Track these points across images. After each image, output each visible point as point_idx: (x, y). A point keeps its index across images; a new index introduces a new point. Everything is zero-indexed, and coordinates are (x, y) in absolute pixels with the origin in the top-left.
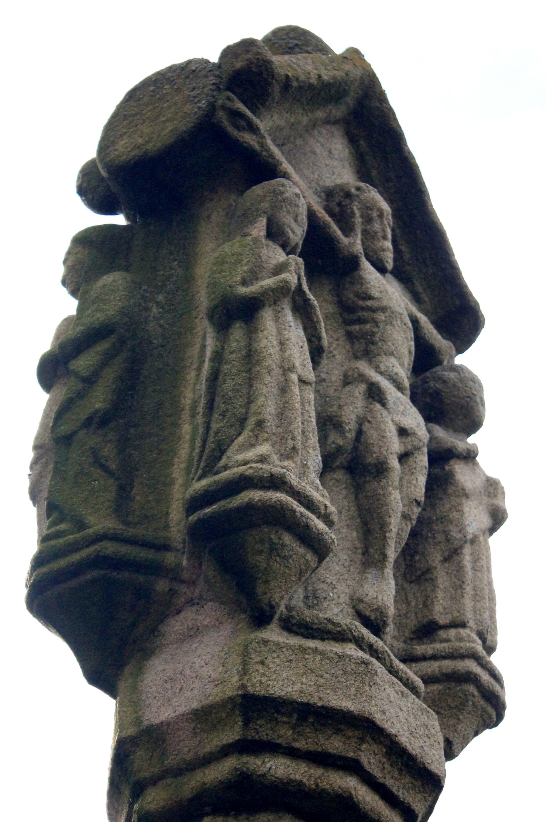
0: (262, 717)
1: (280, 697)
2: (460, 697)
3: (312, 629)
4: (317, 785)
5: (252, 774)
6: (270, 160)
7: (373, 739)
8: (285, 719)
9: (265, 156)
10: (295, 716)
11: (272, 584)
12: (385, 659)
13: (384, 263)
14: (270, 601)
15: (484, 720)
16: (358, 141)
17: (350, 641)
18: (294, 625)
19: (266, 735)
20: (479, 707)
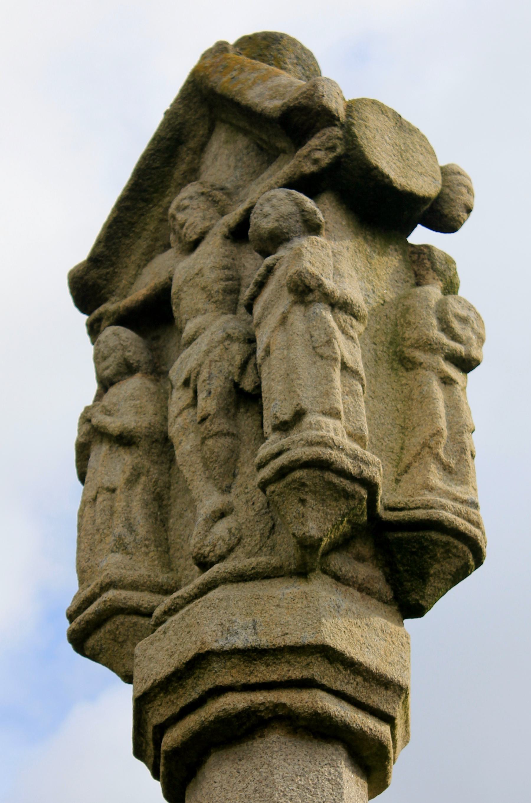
7: (149, 703)
12: (177, 604)
15: (295, 488)
20: (282, 490)
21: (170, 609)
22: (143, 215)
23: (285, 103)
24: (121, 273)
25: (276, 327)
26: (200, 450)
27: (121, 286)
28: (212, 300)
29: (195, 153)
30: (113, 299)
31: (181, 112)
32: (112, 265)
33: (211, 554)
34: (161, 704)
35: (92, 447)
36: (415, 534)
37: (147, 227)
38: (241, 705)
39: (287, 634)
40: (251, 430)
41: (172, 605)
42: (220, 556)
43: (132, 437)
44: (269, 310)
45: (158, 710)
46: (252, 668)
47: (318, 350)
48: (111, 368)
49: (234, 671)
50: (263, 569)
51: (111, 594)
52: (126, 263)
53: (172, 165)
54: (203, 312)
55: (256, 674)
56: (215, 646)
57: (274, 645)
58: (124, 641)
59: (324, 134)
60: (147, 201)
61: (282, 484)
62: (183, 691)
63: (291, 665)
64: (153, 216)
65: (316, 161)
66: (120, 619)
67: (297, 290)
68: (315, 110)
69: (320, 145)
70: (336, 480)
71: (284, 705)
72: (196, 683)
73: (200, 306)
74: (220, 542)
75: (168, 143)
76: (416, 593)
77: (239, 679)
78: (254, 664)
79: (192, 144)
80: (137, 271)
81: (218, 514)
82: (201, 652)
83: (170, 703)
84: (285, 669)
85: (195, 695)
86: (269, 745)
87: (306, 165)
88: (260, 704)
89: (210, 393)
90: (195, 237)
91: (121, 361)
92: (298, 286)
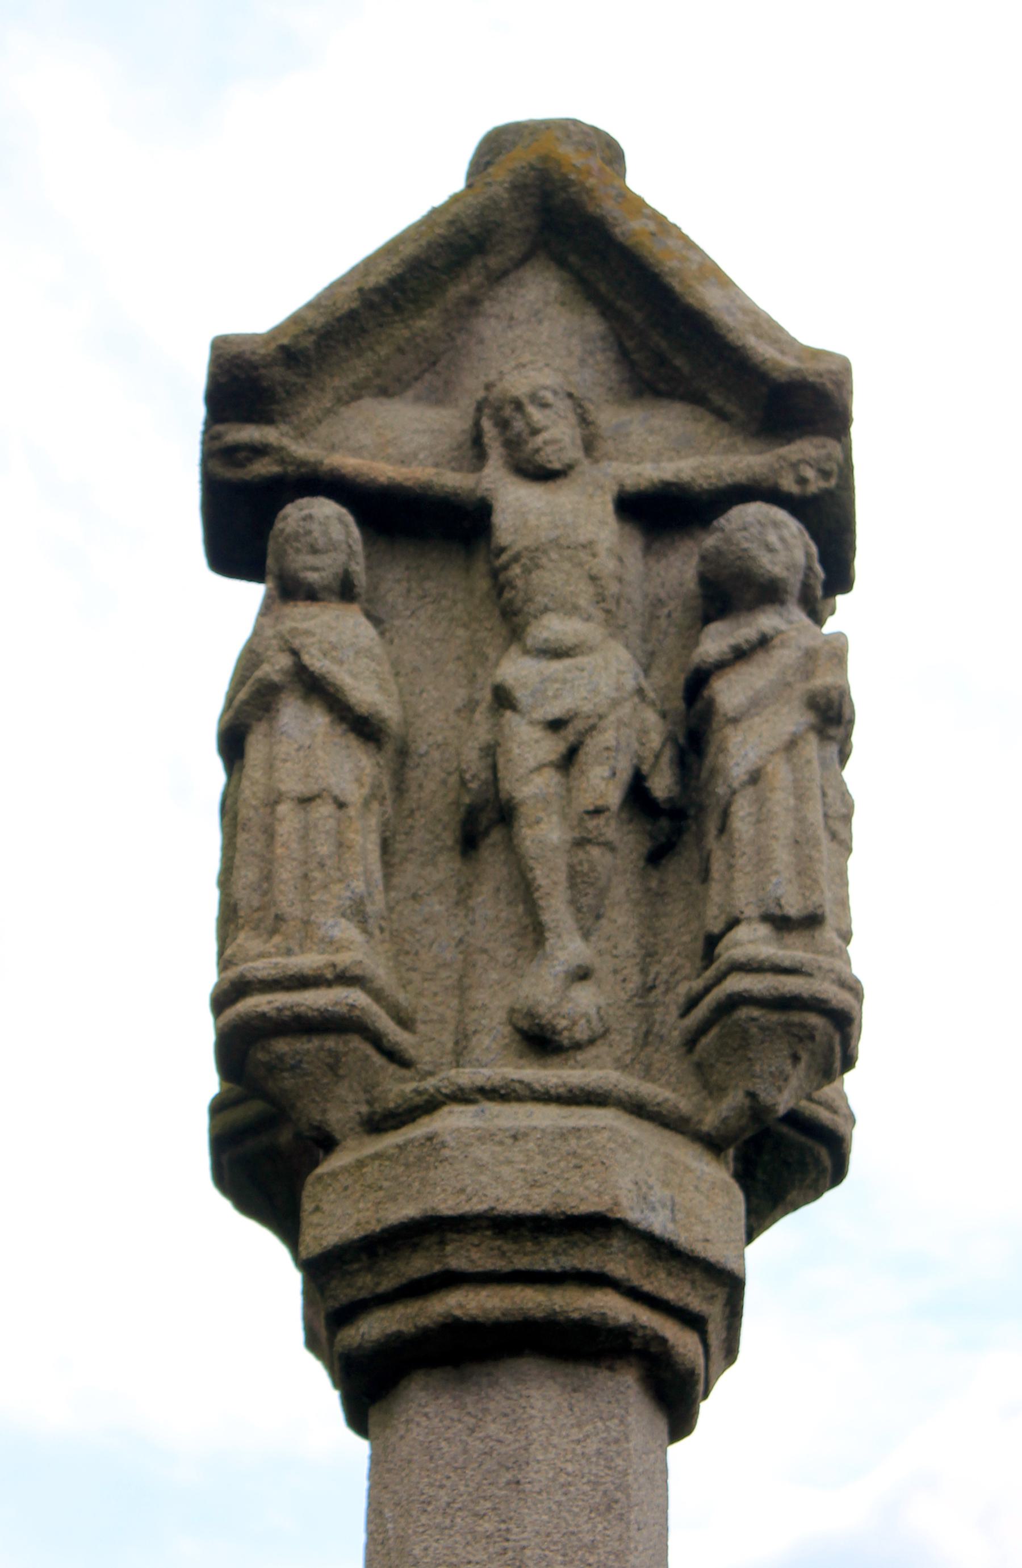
3: (399, 1115)
8: (356, 1266)
10: (364, 1257)
12: (514, 1091)
14: (311, 1124)
15: (794, 1035)
17: (443, 1104)
22: (381, 326)
27: (304, 416)
28: (602, 605)
30: (284, 428)
31: (504, 205)
32: (308, 375)
35: (283, 696)
37: (377, 348)
38: (624, 1319)
41: (502, 1087)
43: (380, 730)
45: (468, 1250)
46: (651, 1269)
48: (324, 574)
49: (631, 1262)
51: (356, 997)
56: (632, 1216)
59: (824, 446)
60: (398, 308)
61: (775, 1017)
64: (392, 336)
65: (802, 481)
66: (357, 1043)
70: (838, 1049)
71: (663, 1341)
72: (564, 1250)
73: (582, 602)
74: (583, 1021)
79: (494, 262)
81: (581, 973)
82: (610, 1215)
84: (686, 1290)
85: (553, 1265)
86: (622, 1389)
89: (614, 774)
90: (557, 466)
91: (340, 571)
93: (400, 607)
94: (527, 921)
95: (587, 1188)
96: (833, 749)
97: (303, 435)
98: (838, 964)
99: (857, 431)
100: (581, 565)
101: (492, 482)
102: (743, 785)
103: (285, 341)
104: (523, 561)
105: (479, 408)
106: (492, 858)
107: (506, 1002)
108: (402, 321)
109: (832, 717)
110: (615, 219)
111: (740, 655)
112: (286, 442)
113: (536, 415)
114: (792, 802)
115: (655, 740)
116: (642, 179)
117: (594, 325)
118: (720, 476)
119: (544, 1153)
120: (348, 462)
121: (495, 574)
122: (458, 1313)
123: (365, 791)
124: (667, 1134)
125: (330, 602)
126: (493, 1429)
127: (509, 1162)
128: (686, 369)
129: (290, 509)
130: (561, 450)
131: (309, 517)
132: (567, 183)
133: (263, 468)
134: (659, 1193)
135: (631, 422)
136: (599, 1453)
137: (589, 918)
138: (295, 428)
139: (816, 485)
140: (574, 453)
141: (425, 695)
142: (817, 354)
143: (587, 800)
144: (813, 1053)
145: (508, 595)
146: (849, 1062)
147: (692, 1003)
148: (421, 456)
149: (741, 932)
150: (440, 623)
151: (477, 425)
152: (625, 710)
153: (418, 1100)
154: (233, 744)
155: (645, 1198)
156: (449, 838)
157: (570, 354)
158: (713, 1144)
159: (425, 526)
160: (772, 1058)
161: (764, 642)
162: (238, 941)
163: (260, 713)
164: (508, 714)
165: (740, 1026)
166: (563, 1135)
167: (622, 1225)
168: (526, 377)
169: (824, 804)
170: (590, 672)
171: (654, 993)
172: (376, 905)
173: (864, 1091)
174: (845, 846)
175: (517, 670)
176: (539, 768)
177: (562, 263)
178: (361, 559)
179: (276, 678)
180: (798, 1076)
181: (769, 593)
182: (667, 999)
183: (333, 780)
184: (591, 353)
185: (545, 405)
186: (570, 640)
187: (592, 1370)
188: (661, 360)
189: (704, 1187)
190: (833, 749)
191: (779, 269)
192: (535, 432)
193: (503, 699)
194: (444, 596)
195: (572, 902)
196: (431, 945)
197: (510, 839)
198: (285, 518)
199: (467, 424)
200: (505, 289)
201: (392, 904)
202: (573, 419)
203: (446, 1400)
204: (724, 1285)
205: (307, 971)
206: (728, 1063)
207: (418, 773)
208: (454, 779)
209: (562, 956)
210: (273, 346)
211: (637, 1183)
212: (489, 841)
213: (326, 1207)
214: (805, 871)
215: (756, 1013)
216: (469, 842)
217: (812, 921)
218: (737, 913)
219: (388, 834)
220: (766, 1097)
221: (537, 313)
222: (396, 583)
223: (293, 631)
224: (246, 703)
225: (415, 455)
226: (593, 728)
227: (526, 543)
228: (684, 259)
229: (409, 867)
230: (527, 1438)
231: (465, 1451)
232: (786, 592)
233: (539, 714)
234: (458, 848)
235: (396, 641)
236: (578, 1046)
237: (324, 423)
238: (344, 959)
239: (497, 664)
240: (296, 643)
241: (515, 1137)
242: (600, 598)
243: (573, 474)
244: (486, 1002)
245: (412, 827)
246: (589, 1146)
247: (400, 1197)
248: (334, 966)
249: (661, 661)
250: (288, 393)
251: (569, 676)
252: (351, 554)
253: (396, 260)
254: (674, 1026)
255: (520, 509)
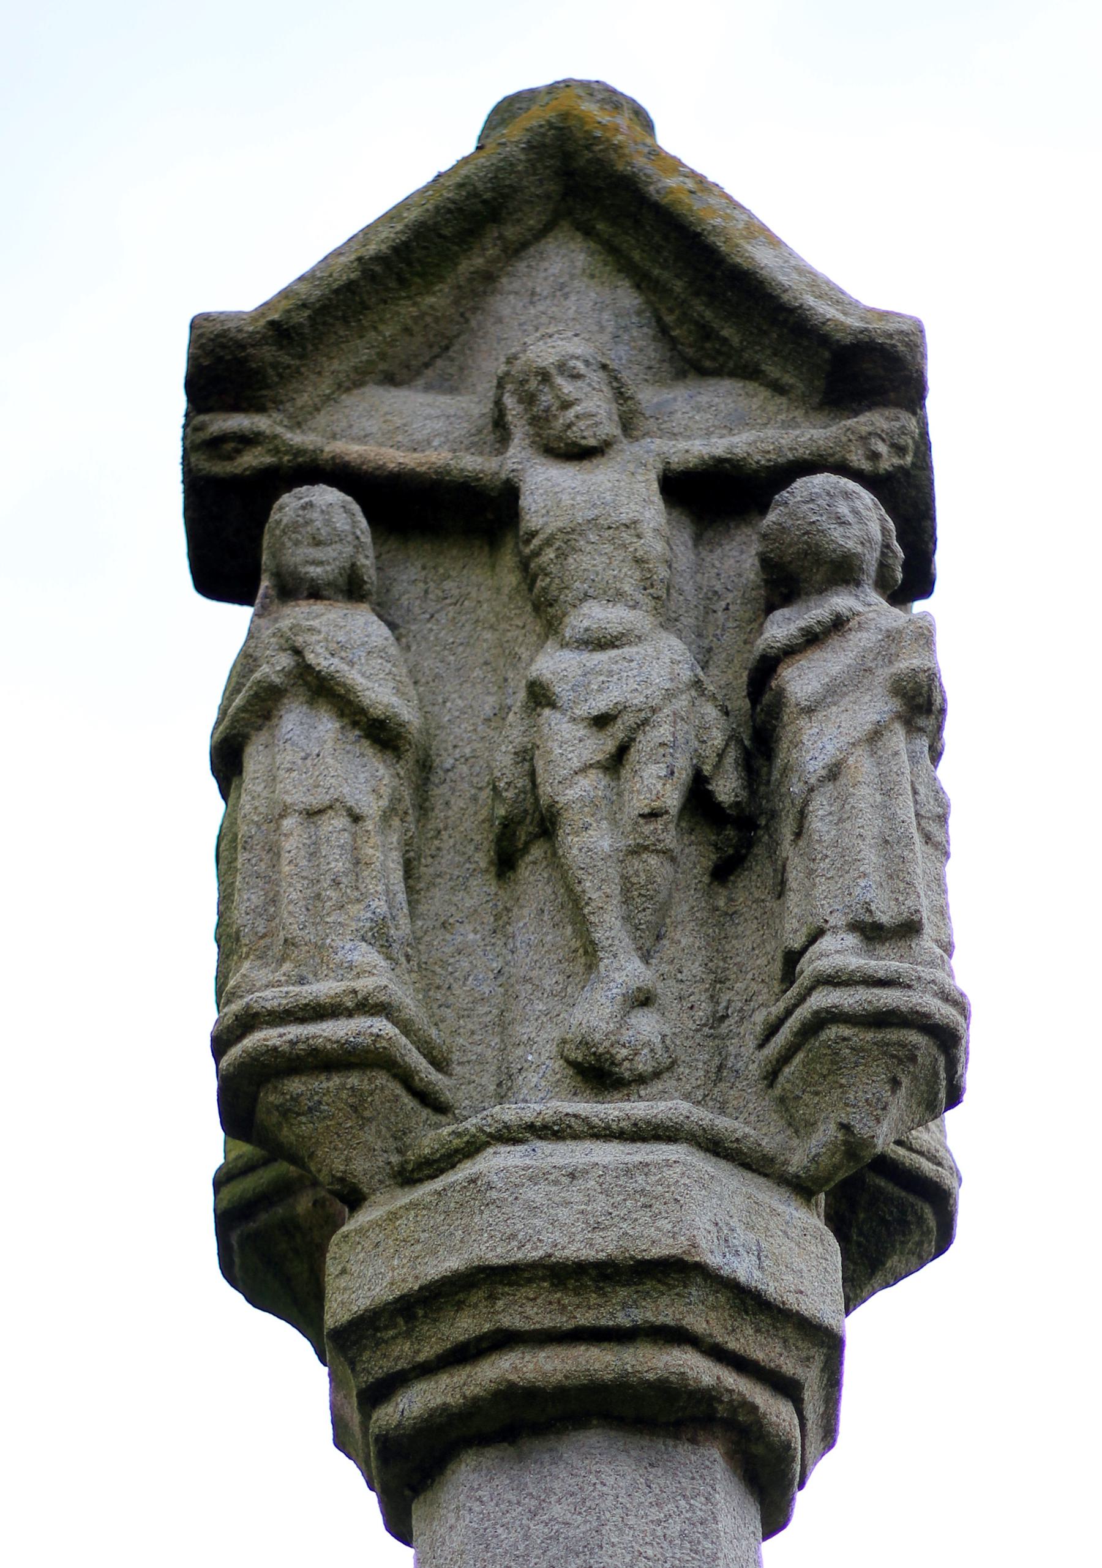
0: (365, 1348)
1: (366, 1310)
2: (825, 1055)
3: (435, 1161)
4: (465, 1397)
5: (388, 1431)
6: (300, 459)
7: (510, 1284)
8: (391, 1333)
9: (289, 461)
10: (400, 1321)
11: (320, 1153)
12: (570, 1126)
13: (580, 445)
14: (333, 1176)
15: (893, 1056)
16: (594, 228)
17: (488, 1144)
18: (413, 1171)
19: (381, 1368)
21: (545, 1127)
22: (385, 302)
23: (866, 329)
24: (306, 378)
25: (860, 740)
26: (622, 862)
27: (299, 403)
28: (651, 591)
29: (505, 250)
32: (302, 357)
33: (626, 1064)
34: (535, 1299)
36: (903, 1194)
38: (707, 1380)
39: (801, 1292)
40: (691, 869)
41: (554, 1123)
42: (640, 1075)
43: (399, 736)
44: (836, 698)
47: (923, 822)
49: (713, 1315)
50: (750, 1148)
51: (381, 1025)
52: (322, 367)
53: (465, 247)
54: (631, 603)
55: (738, 1336)
56: (714, 1261)
57: (783, 1303)
58: (370, 1120)
59: (898, 419)
61: (870, 1036)
62: (598, 1301)
63: (785, 1347)
64: (399, 314)
65: (875, 456)
66: (381, 1078)
67: (913, 698)
68: (907, 373)
69: (887, 434)
71: (754, 1408)
72: (635, 1302)
73: (627, 588)
74: (646, 1051)
75: (480, 207)
76: (853, 1285)
77: (715, 1333)
78: (743, 1319)
79: (511, 232)
80: (333, 393)
83: (555, 1306)
84: (778, 1350)
85: (623, 1320)
86: (707, 1463)
87: (856, 454)
88: (727, 1390)
90: (592, 442)
92: (921, 694)
93: (417, 610)
94: (576, 944)
95: (658, 1229)
96: (923, 743)
97: (299, 425)
98: (940, 975)
99: (932, 403)
100: (625, 546)
101: (519, 463)
102: (822, 781)
103: (276, 316)
104: (558, 544)
105: (500, 386)
106: (533, 878)
107: (556, 1034)
108: (409, 297)
109: (920, 706)
110: (648, 176)
111: (812, 639)
112: (279, 430)
113: (567, 387)
114: (879, 798)
115: (717, 738)
116: (672, 137)
117: (628, 298)
118: (779, 450)
119: (606, 1193)
120: (352, 450)
121: (524, 565)
122: (513, 1377)
123: (384, 803)
124: (749, 1175)
125: (337, 601)
126: (557, 1510)
127: (567, 1203)
128: (736, 341)
129: (286, 498)
130: (596, 424)
131: (310, 505)
132: (592, 140)
133: (252, 459)
134: (742, 1237)
135: (675, 399)
136: (683, 1535)
137: (649, 942)
138: (290, 417)
139: (888, 462)
140: (610, 428)
141: (448, 704)
142: (884, 315)
143: (640, 803)
144: (915, 1078)
145: (540, 584)
146: (955, 1097)
147: (772, 1030)
148: (435, 443)
149: (826, 943)
150: (463, 625)
151: (498, 403)
152: (682, 703)
153: (457, 1142)
154: (227, 761)
155: (726, 1241)
156: (482, 860)
157: (602, 329)
158: (802, 1188)
159: (440, 516)
160: (868, 1083)
161: (838, 624)
162: (243, 971)
163: (260, 721)
164: (547, 712)
165: (829, 1047)
166: (628, 1172)
167: (701, 1269)
168: (554, 347)
169: (916, 802)
170: (634, 665)
171: (727, 1023)
172: (401, 929)
173: (969, 1140)
174: (943, 852)
175: (554, 664)
176: (584, 769)
177: (588, 232)
178: (371, 553)
179: (277, 680)
180: (899, 1104)
181: (843, 572)
182: (742, 1030)
183: (346, 790)
184: (626, 329)
185: (576, 377)
186: (615, 629)
187: (670, 1443)
188: (706, 333)
189: (794, 1233)
190: (923, 743)
191: (834, 231)
192: (566, 405)
193: (540, 696)
194: (467, 596)
195: (627, 919)
196: (466, 979)
197: (555, 854)
198: (281, 508)
199: (487, 407)
200: (525, 264)
201: (419, 934)
202: (608, 393)
203: (502, 1481)
204: (822, 1344)
205: (323, 999)
206: (817, 1093)
207: (444, 789)
208: (486, 793)
209: (619, 977)
210: (262, 322)
211: (717, 1224)
212: (529, 858)
213: (354, 1268)
214: (897, 874)
215: (846, 1031)
216: (505, 862)
217: (910, 929)
218: (821, 923)
219: (412, 854)
220: (861, 1129)
221: (562, 286)
222: (412, 577)
223: (295, 628)
224: (242, 709)
225: (429, 442)
226: (645, 722)
227: (560, 524)
228: (728, 217)
229: (436, 892)
230: (599, 1518)
231: (526, 1537)
232: (861, 569)
233: (581, 711)
234: (493, 869)
235: (413, 648)
236: (641, 1080)
237: (323, 412)
238: (365, 985)
239: (532, 660)
240: (299, 640)
241: (572, 1176)
242: (647, 583)
243: (611, 453)
244: (533, 1035)
245: (439, 849)
246: (659, 1182)
247: (441, 1249)
248: (355, 992)
249: (719, 658)
250: (280, 376)
251: (615, 667)
252: (359, 546)
253: (399, 227)
254: (754, 1062)
255: (550, 492)
